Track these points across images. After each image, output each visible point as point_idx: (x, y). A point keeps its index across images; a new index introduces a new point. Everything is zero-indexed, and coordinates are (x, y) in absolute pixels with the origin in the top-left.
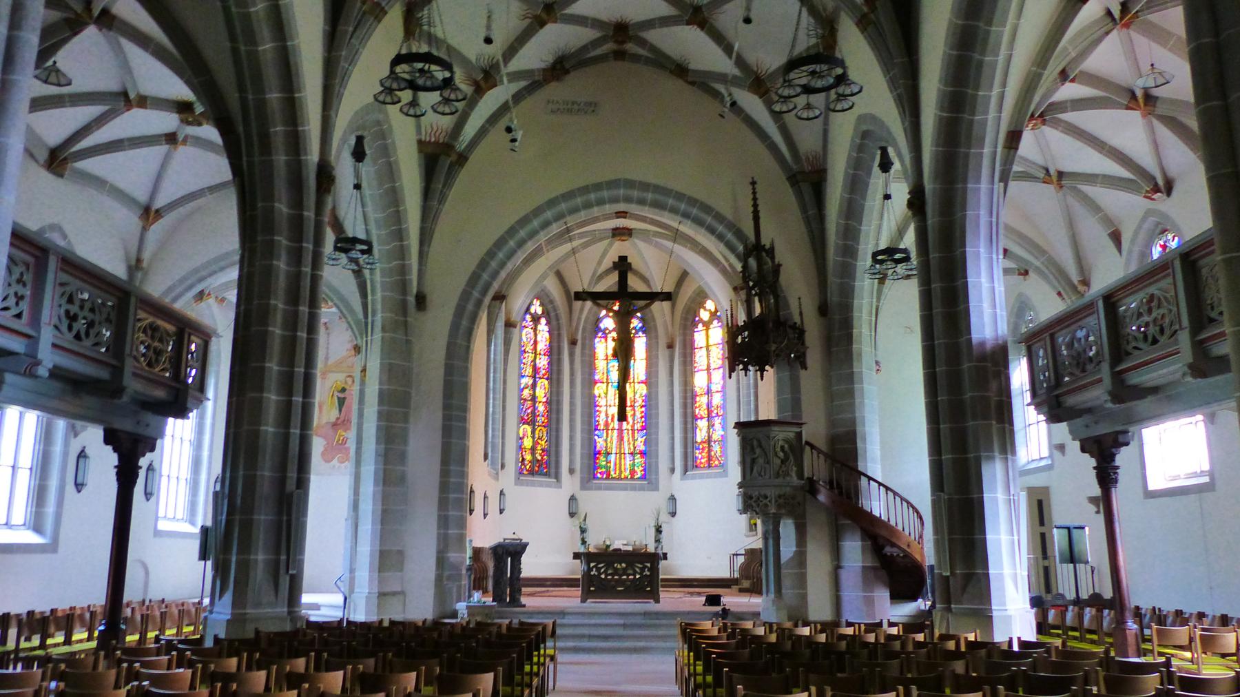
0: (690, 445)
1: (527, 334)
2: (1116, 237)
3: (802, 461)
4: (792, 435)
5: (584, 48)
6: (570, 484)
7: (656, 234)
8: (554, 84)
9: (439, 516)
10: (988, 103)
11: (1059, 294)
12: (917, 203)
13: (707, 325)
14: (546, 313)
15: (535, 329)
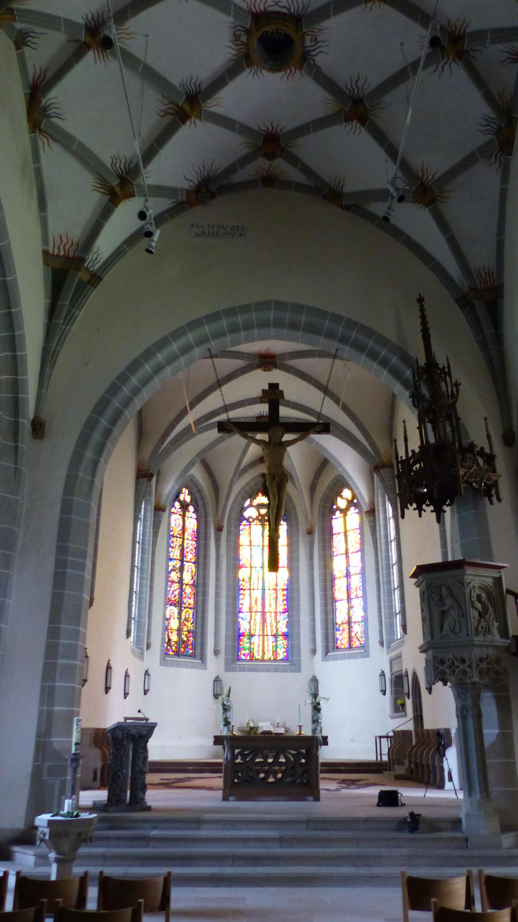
0: (330, 626)
1: (176, 520)
6: (214, 665)
9: (43, 688)
13: (344, 512)
14: (194, 502)
15: (184, 516)
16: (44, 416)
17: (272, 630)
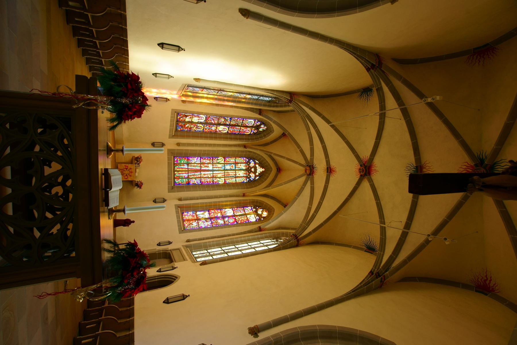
14: (259, 133)
17: (191, 176)
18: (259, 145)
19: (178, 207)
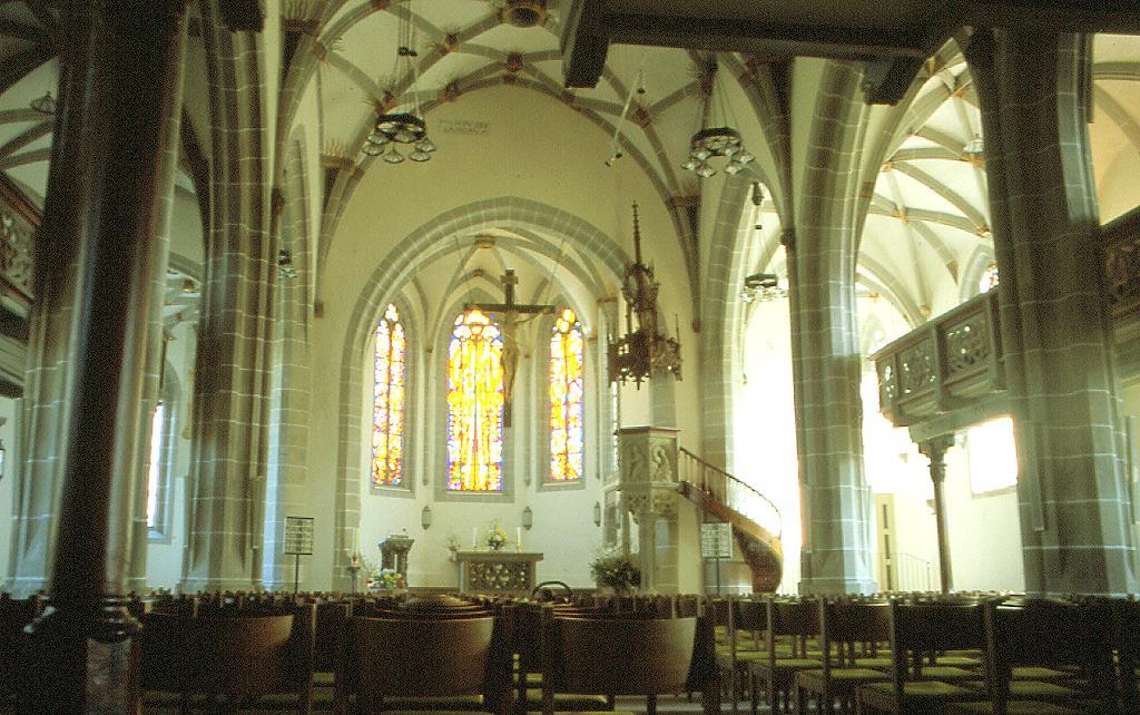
2: (953, 269)
3: (676, 465)
4: (668, 441)
5: (478, 73)
7: (520, 243)
8: (447, 104)
10: (848, 163)
11: (905, 317)
12: (788, 237)
14: (402, 321)
16: (322, 299)
18: (426, 328)
19: (540, 488)
